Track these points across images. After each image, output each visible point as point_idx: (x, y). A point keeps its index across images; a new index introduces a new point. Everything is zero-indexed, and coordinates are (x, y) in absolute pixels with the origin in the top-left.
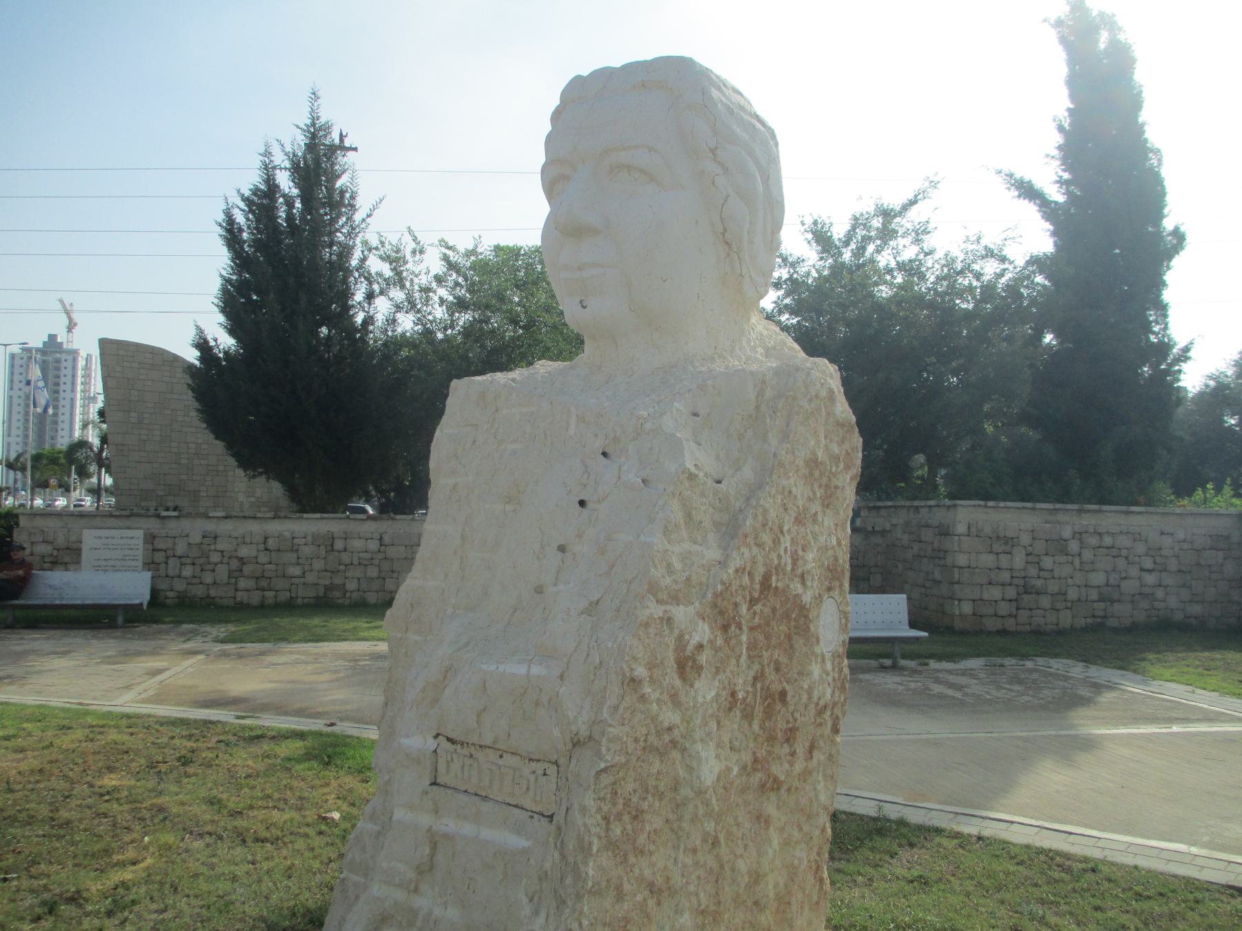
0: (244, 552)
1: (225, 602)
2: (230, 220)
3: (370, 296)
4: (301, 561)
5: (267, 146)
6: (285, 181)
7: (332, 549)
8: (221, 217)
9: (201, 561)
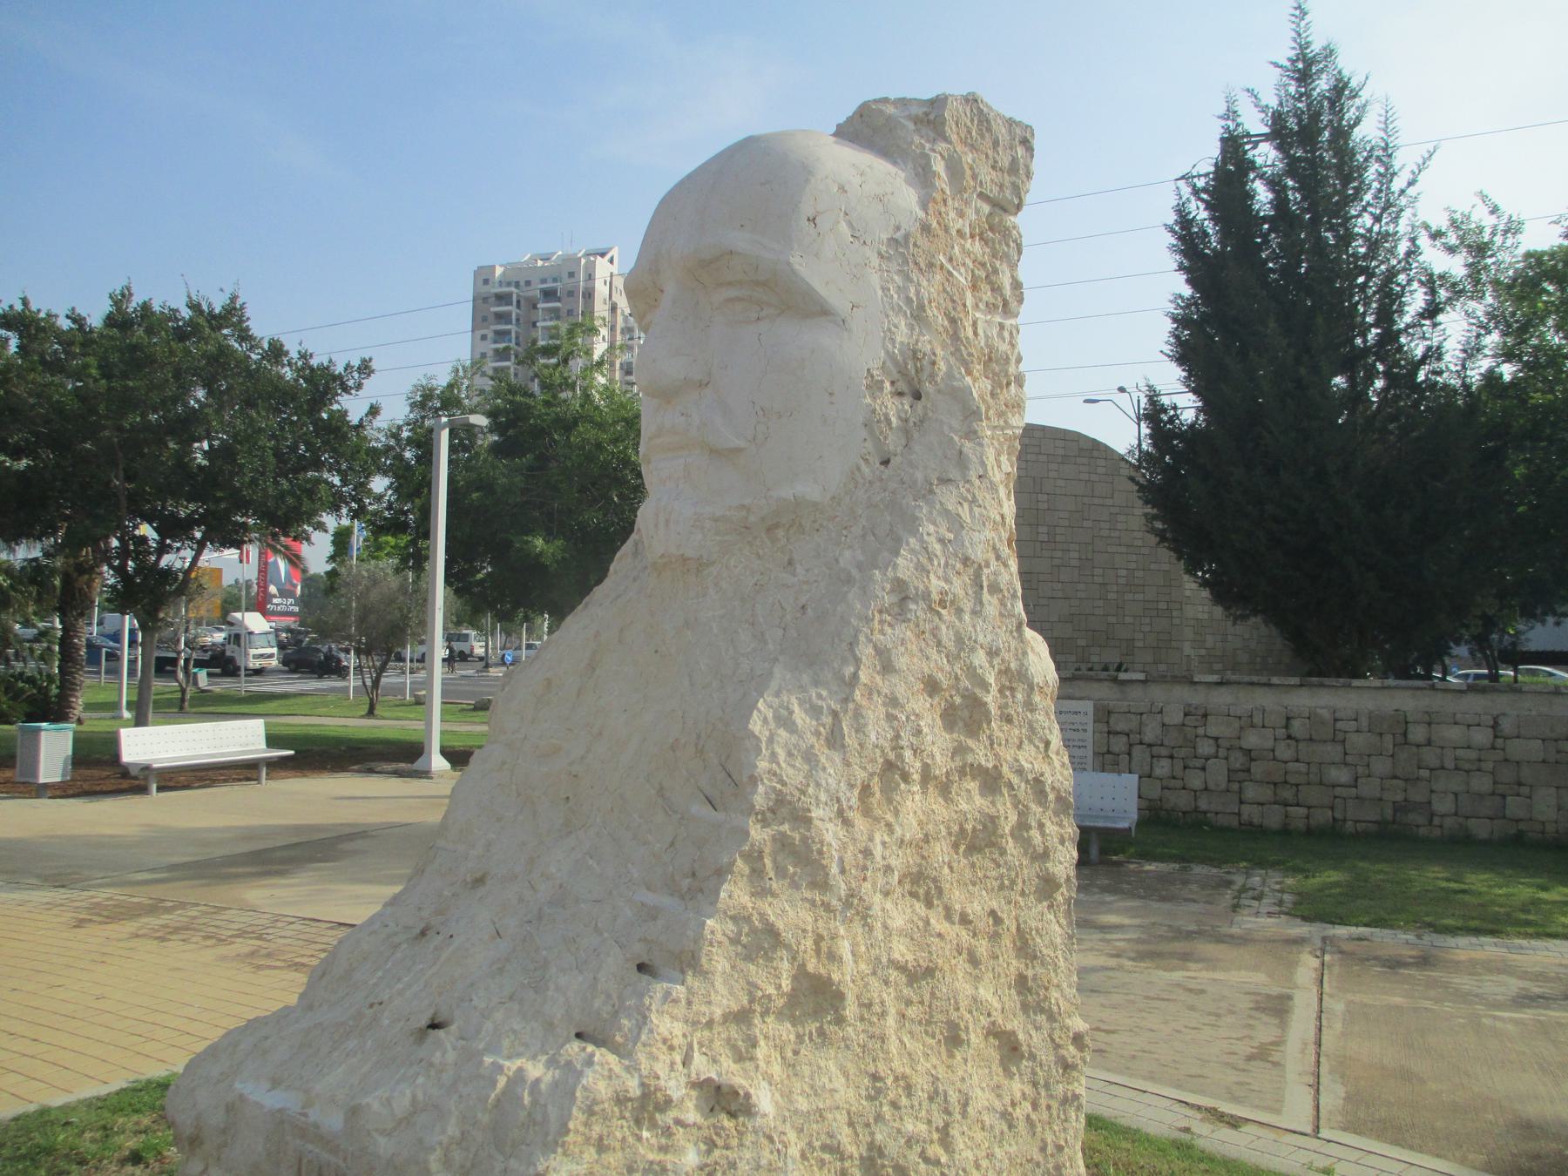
0: (1252, 740)
1: (1222, 821)
2: (1185, 221)
3: (1432, 311)
4: (1349, 759)
5: (1230, 102)
6: (1266, 155)
7: (1404, 740)
8: (1171, 218)
9: (1183, 752)
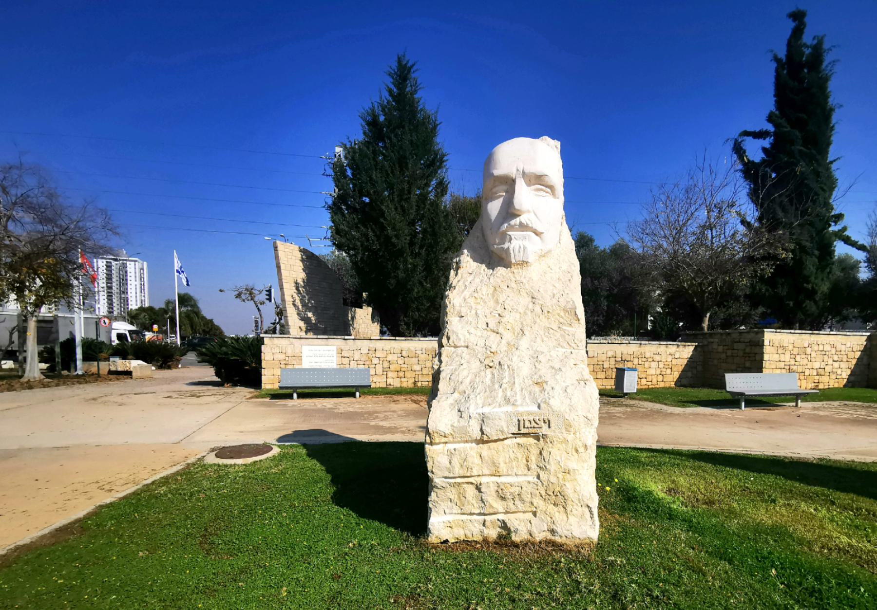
0: (390, 358)
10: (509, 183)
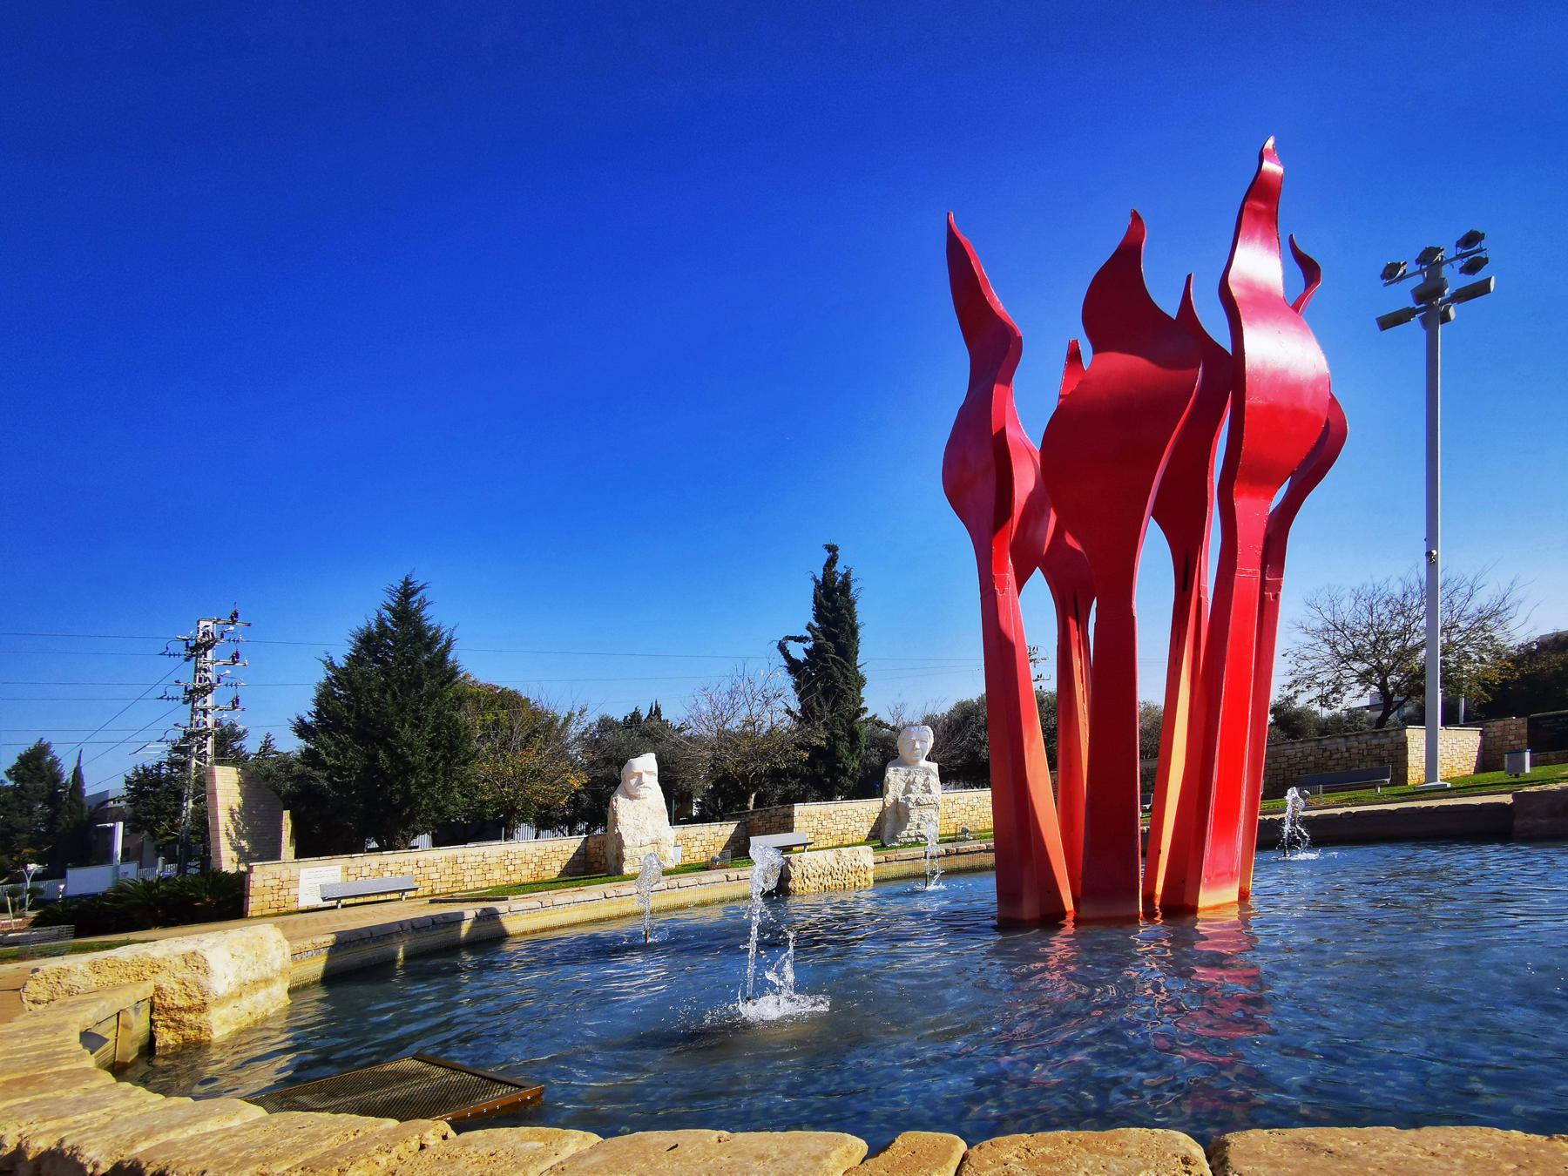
0: (404, 869)
10: (640, 775)
